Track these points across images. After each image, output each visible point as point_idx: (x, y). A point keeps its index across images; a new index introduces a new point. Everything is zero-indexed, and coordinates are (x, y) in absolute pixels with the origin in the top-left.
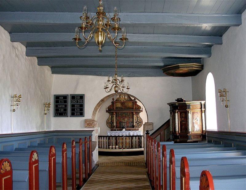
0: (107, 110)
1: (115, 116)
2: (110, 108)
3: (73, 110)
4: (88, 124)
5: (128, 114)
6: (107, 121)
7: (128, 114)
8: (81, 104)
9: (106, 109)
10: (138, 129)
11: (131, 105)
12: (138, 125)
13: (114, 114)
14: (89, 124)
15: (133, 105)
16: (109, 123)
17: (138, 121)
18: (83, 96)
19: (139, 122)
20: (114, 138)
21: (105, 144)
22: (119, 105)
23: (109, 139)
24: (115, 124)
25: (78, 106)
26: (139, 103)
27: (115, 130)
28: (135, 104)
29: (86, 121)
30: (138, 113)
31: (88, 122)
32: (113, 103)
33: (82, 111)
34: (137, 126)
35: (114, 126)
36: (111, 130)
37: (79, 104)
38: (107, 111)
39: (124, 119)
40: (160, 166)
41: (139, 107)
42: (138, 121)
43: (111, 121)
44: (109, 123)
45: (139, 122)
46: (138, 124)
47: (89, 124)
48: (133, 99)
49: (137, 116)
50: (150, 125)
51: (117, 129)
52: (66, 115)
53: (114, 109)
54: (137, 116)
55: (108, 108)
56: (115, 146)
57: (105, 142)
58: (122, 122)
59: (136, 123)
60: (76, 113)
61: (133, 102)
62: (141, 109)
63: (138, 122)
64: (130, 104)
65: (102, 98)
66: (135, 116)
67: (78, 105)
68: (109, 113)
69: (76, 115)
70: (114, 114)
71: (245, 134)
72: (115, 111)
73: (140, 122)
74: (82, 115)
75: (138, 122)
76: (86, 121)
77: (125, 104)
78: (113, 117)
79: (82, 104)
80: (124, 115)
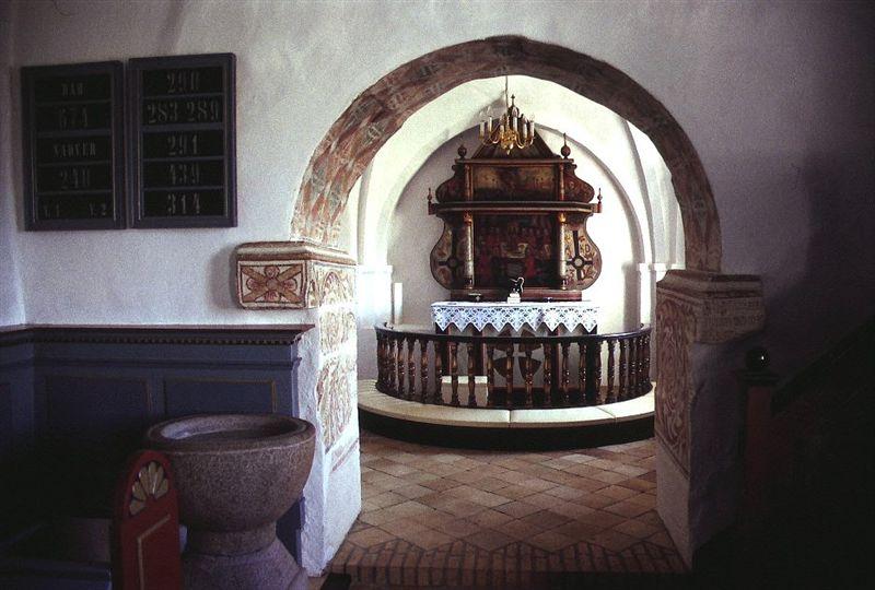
0: (434, 201)
1: (470, 230)
2: (447, 193)
3: (155, 175)
4: (258, 283)
5: (534, 221)
6: (436, 254)
7: (534, 221)
8: (203, 127)
9: (430, 197)
10: (580, 295)
11: (545, 179)
12: (579, 274)
13: (467, 223)
14: (268, 278)
15: (557, 179)
16: (442, 264)
17: (577, 256)
18: (220, 68)
19: (585, 263)
20: (463, 347)
21: (405, 373)
22: (489, 179)
23: (442, 351)
24: (471, 271)
25: (190, 144)
26: (585, 171)
27: (472, 299)
28: (566, 176)
29: (248, 257)
30: (578, 220)
31: (259, 268)
32: (459, 168)
33: (221, 183)
34: (575, 278)
35: (467, 281)
36: (454, 298)
37: (196, 127)
38: (433, 209)
39: (513, 248)
40: (539, 295)
41: (585, 191)
42: (577, 256)
43: (453, 256)
44: (442, 264)
45: (585, 263)
46: (579, 269)
47: (268, 278)
48: (556, 148)
49: (575, 233)
50: (741, 293)
51: (477, 294)
52: (110, 214)
53: (463, 197)
54: (575, 233)
55: (438, 192)
56: (472, 380)
57: (417, 369)
58: (507, 261)
59: (568, 263)
60: (179, 195)
61: (556, 167)
62: (595, 201)
63: (578, 262)
64: (543, 176)
65: (367, 79)
66: (565, 235)
67: (190, 134)
68: (439, 215)
69: (179, 212)
70: (467, 223)
71: (757, 284)
72: (472, 205)
73: (590, 263)
74: (222, 213)
75: (578, 262)
76: (238, 258)
77: (521, 174)
78: (464, 234)
79: (214, 126)
80: (514, 226)
